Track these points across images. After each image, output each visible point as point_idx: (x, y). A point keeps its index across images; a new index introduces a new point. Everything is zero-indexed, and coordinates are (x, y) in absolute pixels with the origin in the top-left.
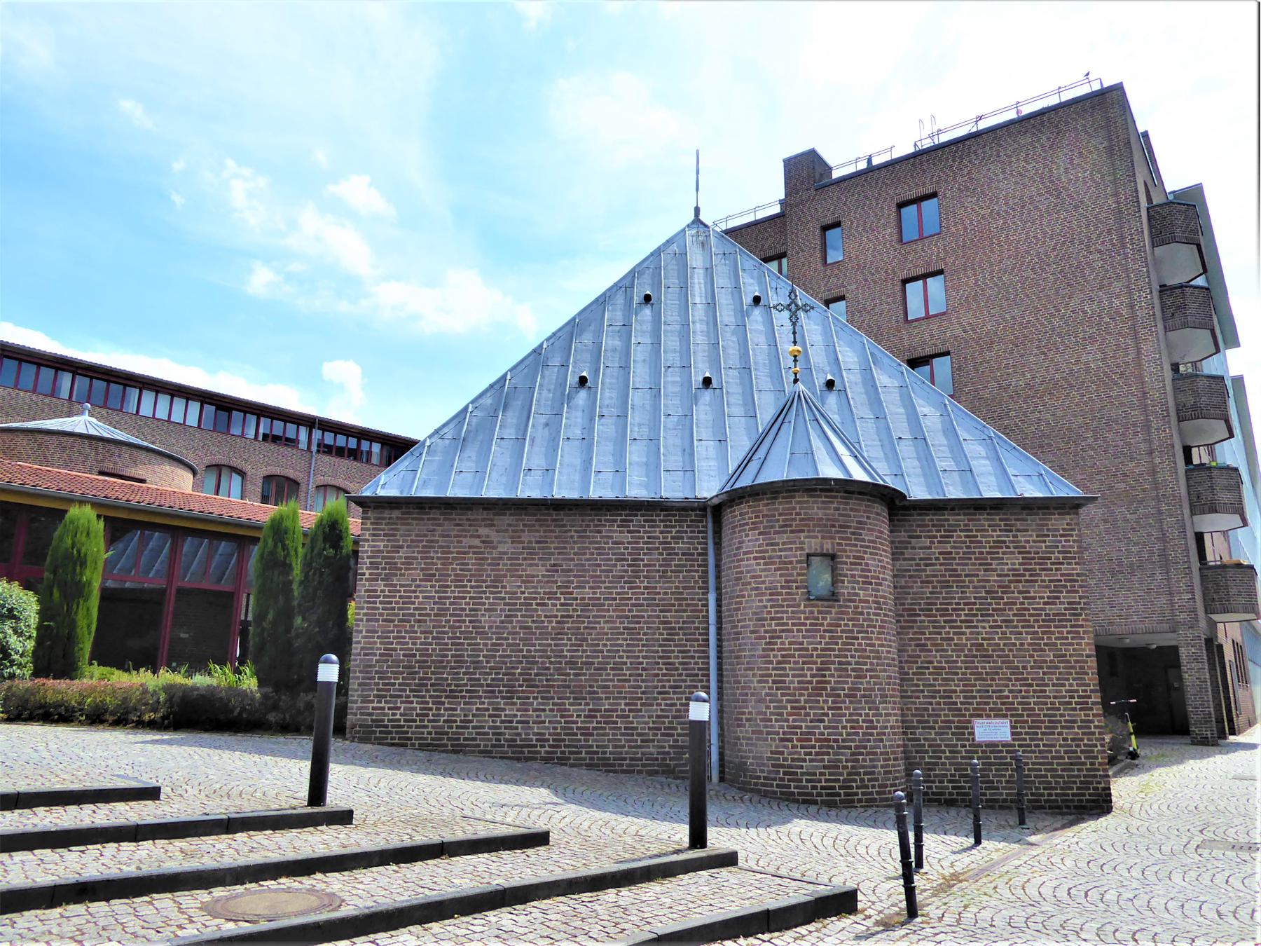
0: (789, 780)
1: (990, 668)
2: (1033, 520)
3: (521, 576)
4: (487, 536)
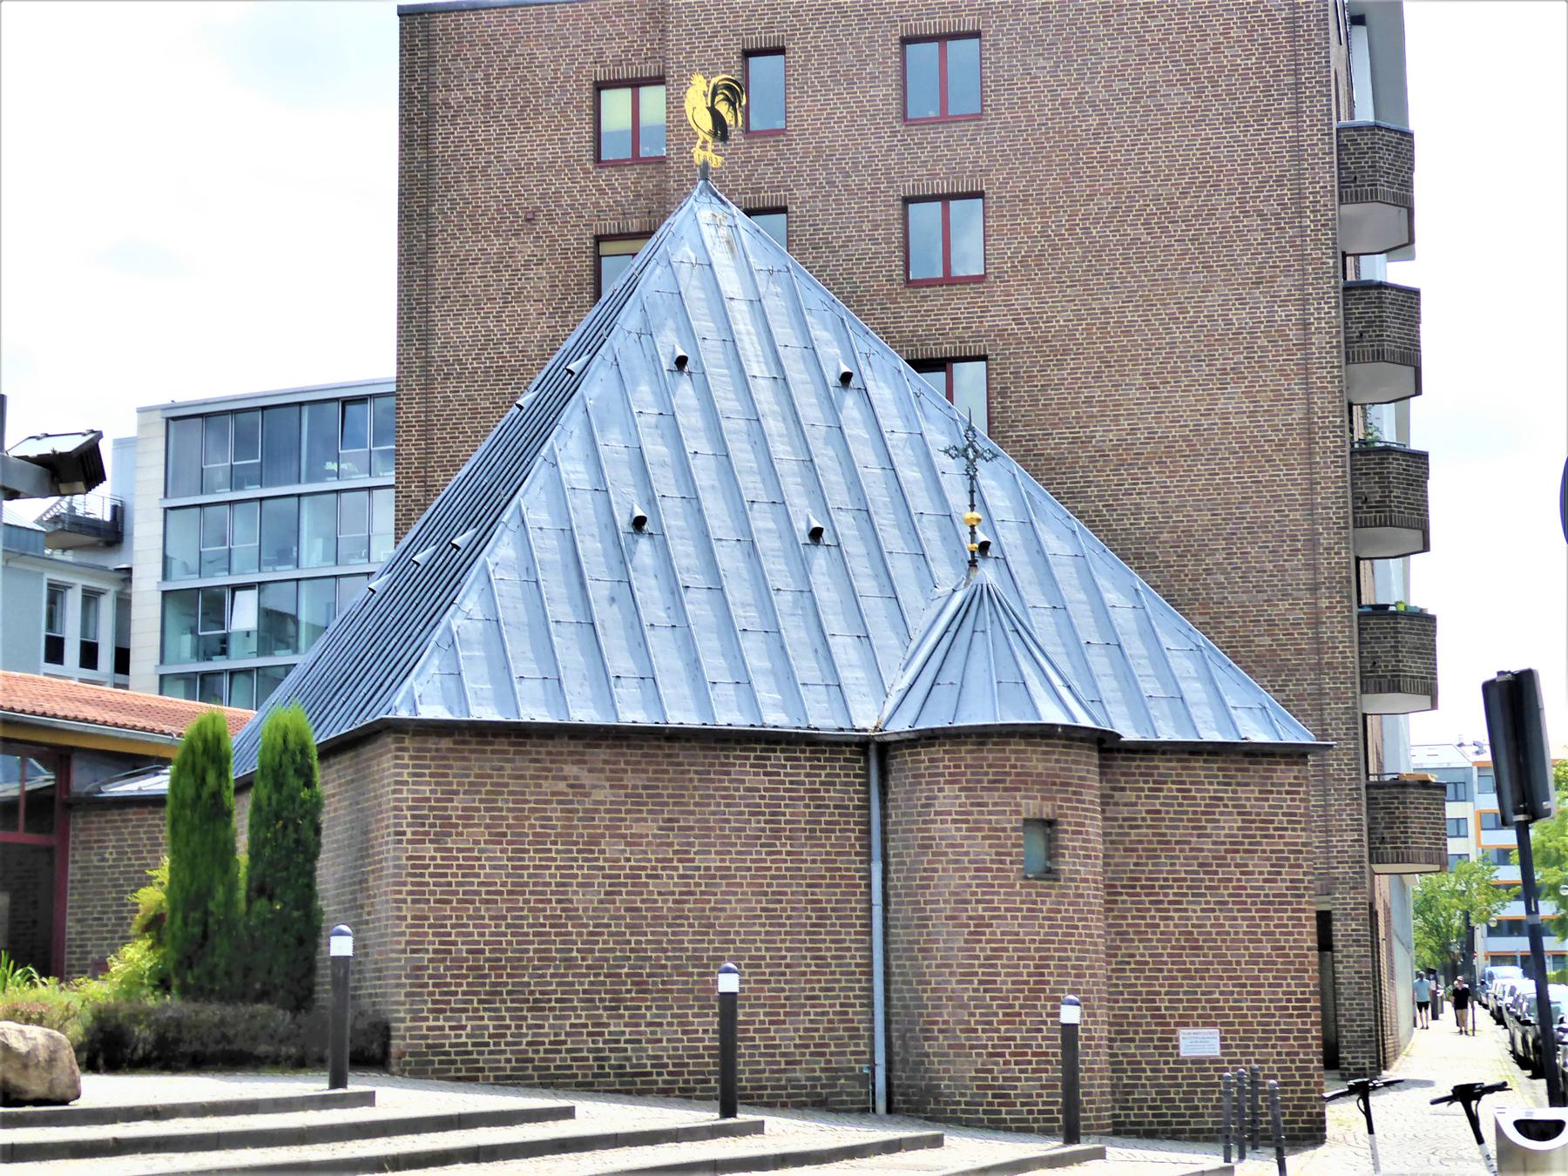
0: (1000, 1104)
1: (1201, 963)
2: (1258, 770)
3: (624, 836)
4: (576, 778)
